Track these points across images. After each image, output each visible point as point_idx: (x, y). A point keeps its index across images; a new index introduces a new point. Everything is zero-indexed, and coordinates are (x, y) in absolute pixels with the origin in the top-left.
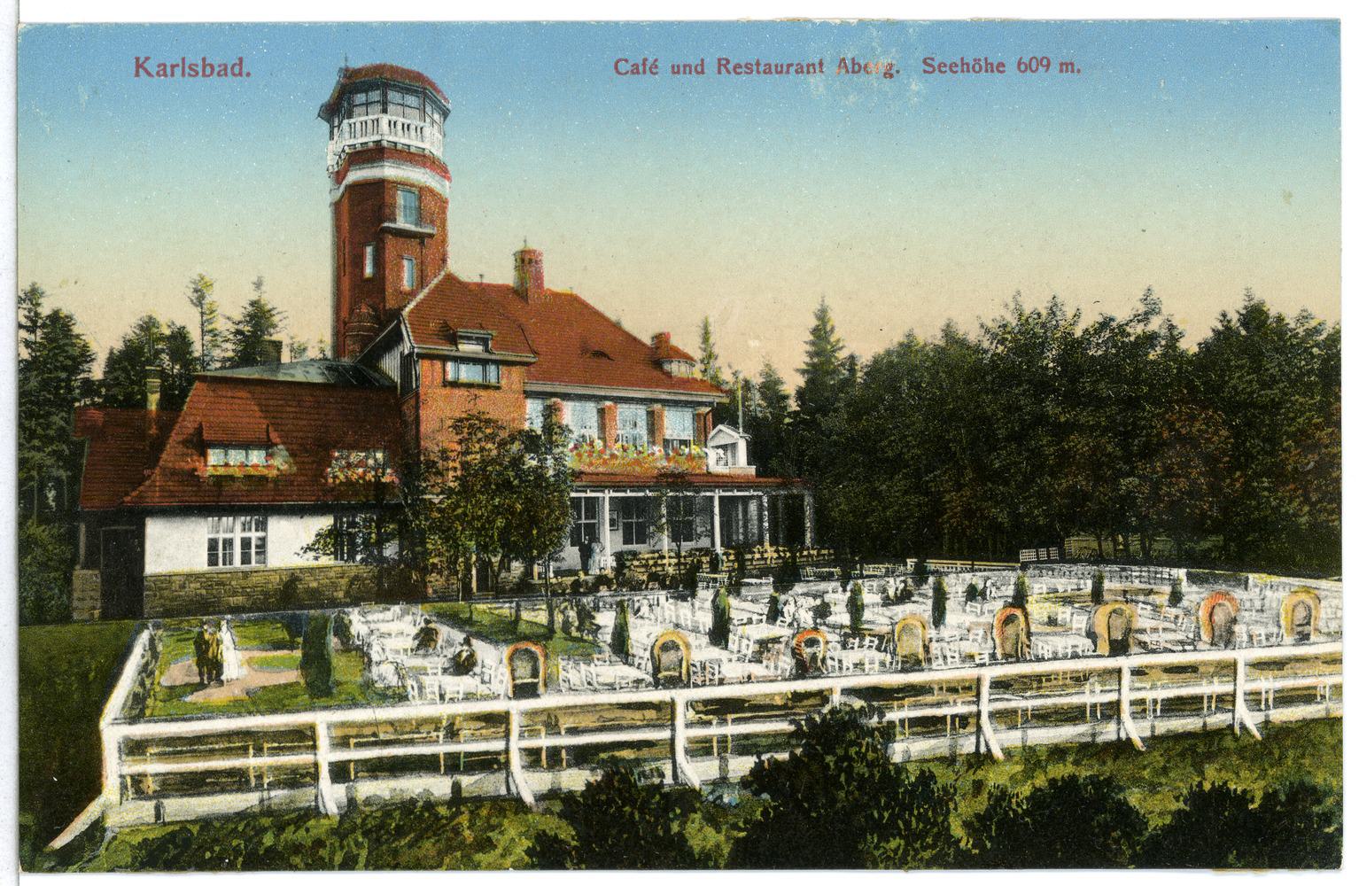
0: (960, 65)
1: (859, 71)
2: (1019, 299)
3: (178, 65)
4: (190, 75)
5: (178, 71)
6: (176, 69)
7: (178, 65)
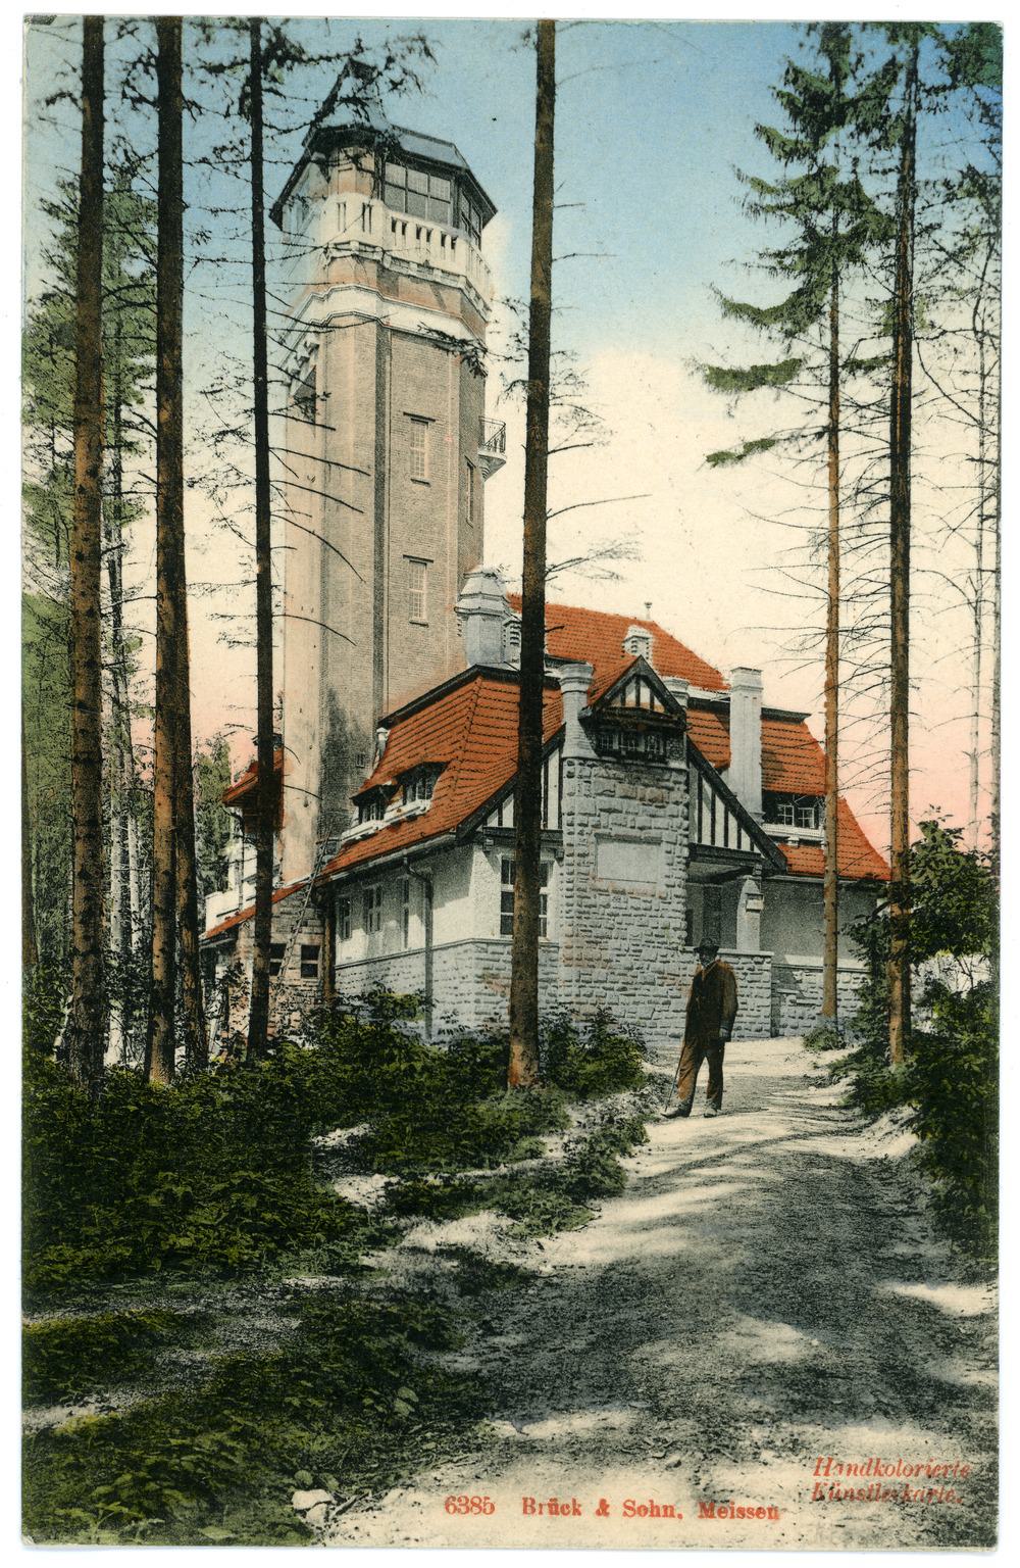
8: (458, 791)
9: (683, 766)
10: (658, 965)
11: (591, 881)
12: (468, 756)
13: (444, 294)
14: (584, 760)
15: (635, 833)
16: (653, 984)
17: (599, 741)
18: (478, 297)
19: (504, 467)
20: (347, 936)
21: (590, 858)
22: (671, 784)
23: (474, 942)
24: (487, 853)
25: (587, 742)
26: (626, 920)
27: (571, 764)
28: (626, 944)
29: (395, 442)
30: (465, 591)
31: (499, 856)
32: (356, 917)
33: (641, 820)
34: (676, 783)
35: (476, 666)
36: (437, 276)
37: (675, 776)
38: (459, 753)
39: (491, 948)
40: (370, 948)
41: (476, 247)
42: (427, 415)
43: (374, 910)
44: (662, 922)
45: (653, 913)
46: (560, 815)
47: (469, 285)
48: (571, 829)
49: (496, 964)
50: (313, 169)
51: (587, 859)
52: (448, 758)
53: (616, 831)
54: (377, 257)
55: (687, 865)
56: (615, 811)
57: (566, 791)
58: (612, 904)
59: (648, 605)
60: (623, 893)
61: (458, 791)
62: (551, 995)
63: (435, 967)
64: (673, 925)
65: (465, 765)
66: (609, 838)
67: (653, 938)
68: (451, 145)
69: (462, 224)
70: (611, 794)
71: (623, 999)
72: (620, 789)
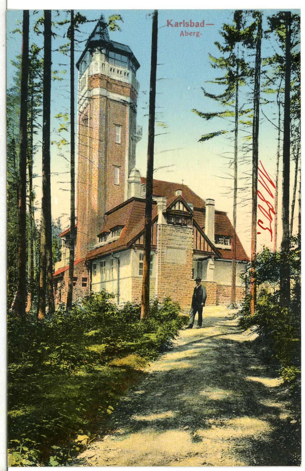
0: (190, 23)
1: (193, 26)
2: (277, 73)
3: (182, 23)
4: (186, 26)
5: (182, 25)
6: (181, 24)
7: (182, 23)
10: (183, 284)
15: (178, 246)
37: (190, 230)
50: (88, 53)
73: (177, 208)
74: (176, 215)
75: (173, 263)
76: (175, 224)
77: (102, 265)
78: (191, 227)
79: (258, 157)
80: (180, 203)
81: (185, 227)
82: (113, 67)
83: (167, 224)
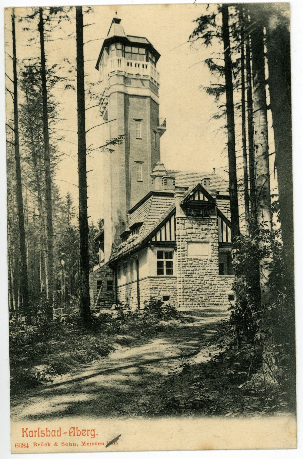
8: (145, 231)
9: (215, 217)
10: (210, 282)
11: (186, 256)
12: (148, 220)
13: (144, 82)
14: (182, 218)
15: (200, 240)
16: (208, 288)
17: (187, 212)
18: (155, 81)
19: (166, 132)
20: (120, 277)
21: (185, 249)
22: (211, 224)
23: (149, 277)
24: (152, 249)
25: (183, 212)
26: (198, 268)
27: (178, 220)
28: (198, 276)
29: (132, 128)
30: (154, 170)
31: (156, 251)
32: (122, 272)
33: (202, 236)
34: (213, 223)
35: (151, 192)
36: (142, 77)
37: (213, 221)
38: (146, 219)
39: (155, 279)
40: (127, 282)
41: (154, 68)
42: (140, 119)
43: (125, 270)
44: (210, 268)
45: (207, 265)
46: (175, 236)
47: (152, 78)
48: (179, 240)
49: (156, 284)
50: (105, 52)
51: (184, 249)
52: (143, 221)
53: (194, 240)
54: (123, 74)
55: (219, 249)
56: (193, 233)
57: (177, 228)
58: (193, 263)
59: (214, 169)
60: (197, 259)
61: (145, 231)
62: (174, 293)
63: (140, 286)
64: (214, 269)
65: (148, 223)
66: (191, 242)
67: (208, 273)
68: (145, 38)
69: (149, 60)
70: (192, 228)
71: (198, 293)
72: (196, 226)
73: (196, 198)
74: (196, 206)
75: (195, 259)
76: (195, 216)
77: (125, 267)
78: (215, 217)
79: (84, 56)
80: (200, 192)
81: (207, 218)
82: (130, 61)
83: (185, 216)
